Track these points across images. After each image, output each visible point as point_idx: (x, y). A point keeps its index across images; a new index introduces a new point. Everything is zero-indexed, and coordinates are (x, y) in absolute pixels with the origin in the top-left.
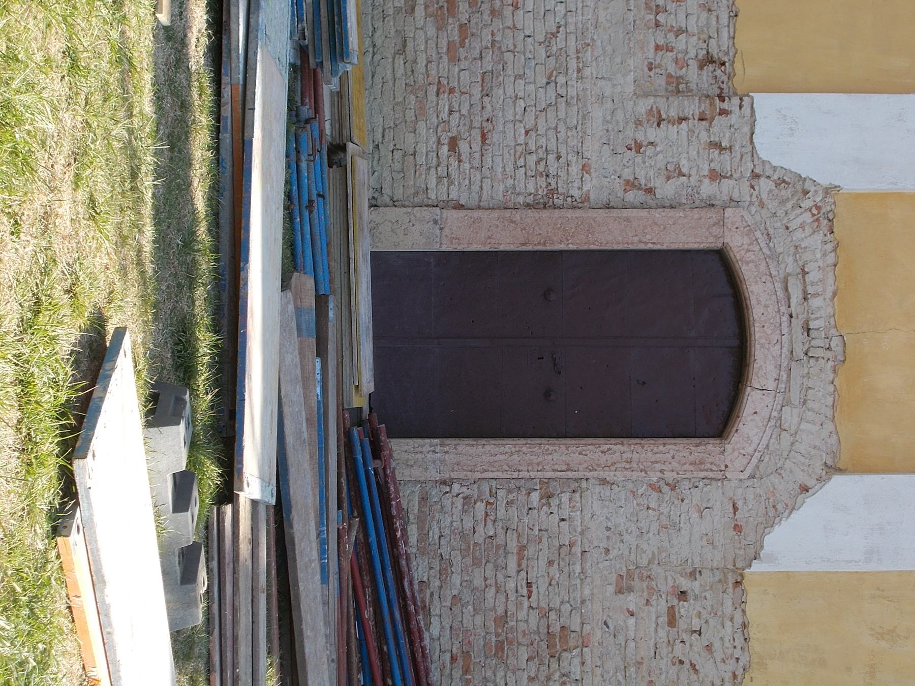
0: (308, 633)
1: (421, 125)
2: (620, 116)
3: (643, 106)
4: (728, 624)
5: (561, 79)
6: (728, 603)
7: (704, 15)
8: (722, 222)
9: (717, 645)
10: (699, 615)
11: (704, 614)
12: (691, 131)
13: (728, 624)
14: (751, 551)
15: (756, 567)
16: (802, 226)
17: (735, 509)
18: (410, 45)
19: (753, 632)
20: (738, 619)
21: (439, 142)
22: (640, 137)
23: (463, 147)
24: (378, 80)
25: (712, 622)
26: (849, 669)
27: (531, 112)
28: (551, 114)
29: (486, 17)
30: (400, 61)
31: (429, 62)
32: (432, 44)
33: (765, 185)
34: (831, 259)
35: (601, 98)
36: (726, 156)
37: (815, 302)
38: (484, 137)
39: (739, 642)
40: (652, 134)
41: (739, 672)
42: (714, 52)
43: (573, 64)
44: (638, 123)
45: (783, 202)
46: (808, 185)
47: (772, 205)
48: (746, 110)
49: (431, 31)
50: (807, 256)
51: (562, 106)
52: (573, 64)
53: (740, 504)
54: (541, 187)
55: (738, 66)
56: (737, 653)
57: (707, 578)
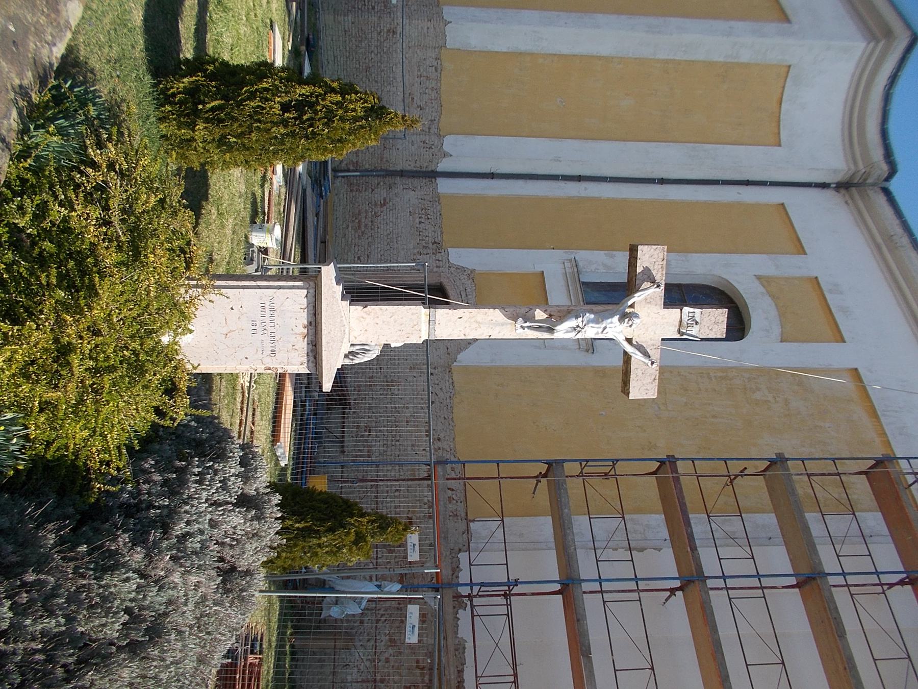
0: (309, 247)
1: (349, 254)
2: (409, 253)
3: (415, 251)
4: (447, 382)
5: (391, 244)
6: (447, 376)
7: (433, 233)
8: (440, 276)
9: (444, 388)
10: (438, 379)
11: (439, 379)
12: (430, 257)
13: (447, 382)
14: (453, 360)
15: (455, 364)
16: (464, 279)
17: (447, 349)
18: (347, 236)
19: (455, 384)
20: (451, 381)
21: (355, 257)
22: (415, 258)
23: (362, 258)
24: (337, 243)
25: (442, 381)
26: (489, 395)
27: (383, 251)
28: (388, 251)
29: (370, 230)
30: (343, 239)
31: (352, 239)
32: (353, 236)
33: (452, 269)
34: (474, 288)
35: (403, 249)
36: (441, 262)
37: (469, 297)
38: (368, 256)
39: (451, 387)
40: (419, 257)
41: (452, 396)
42: (436, 241)
43: (395, 241)
44: (415, 254)
45: (458, 273)
46: (465, 269)
47: (455, 274)
48: (446, 252)
49: (353, 232)
50: (466, 286)
51: (392, 249)
52: (395, 241)
53: (449, 347)
54: (461, 502)
55: (443, 244)
56: (451, 391)
57: (440, 369)
